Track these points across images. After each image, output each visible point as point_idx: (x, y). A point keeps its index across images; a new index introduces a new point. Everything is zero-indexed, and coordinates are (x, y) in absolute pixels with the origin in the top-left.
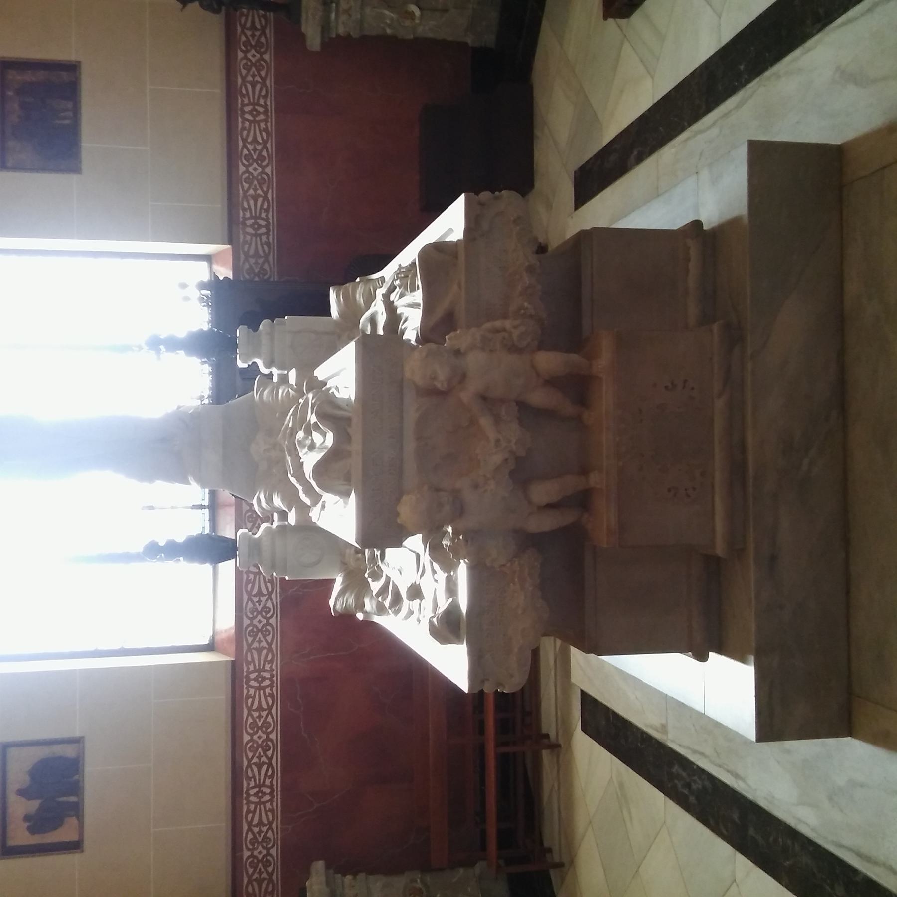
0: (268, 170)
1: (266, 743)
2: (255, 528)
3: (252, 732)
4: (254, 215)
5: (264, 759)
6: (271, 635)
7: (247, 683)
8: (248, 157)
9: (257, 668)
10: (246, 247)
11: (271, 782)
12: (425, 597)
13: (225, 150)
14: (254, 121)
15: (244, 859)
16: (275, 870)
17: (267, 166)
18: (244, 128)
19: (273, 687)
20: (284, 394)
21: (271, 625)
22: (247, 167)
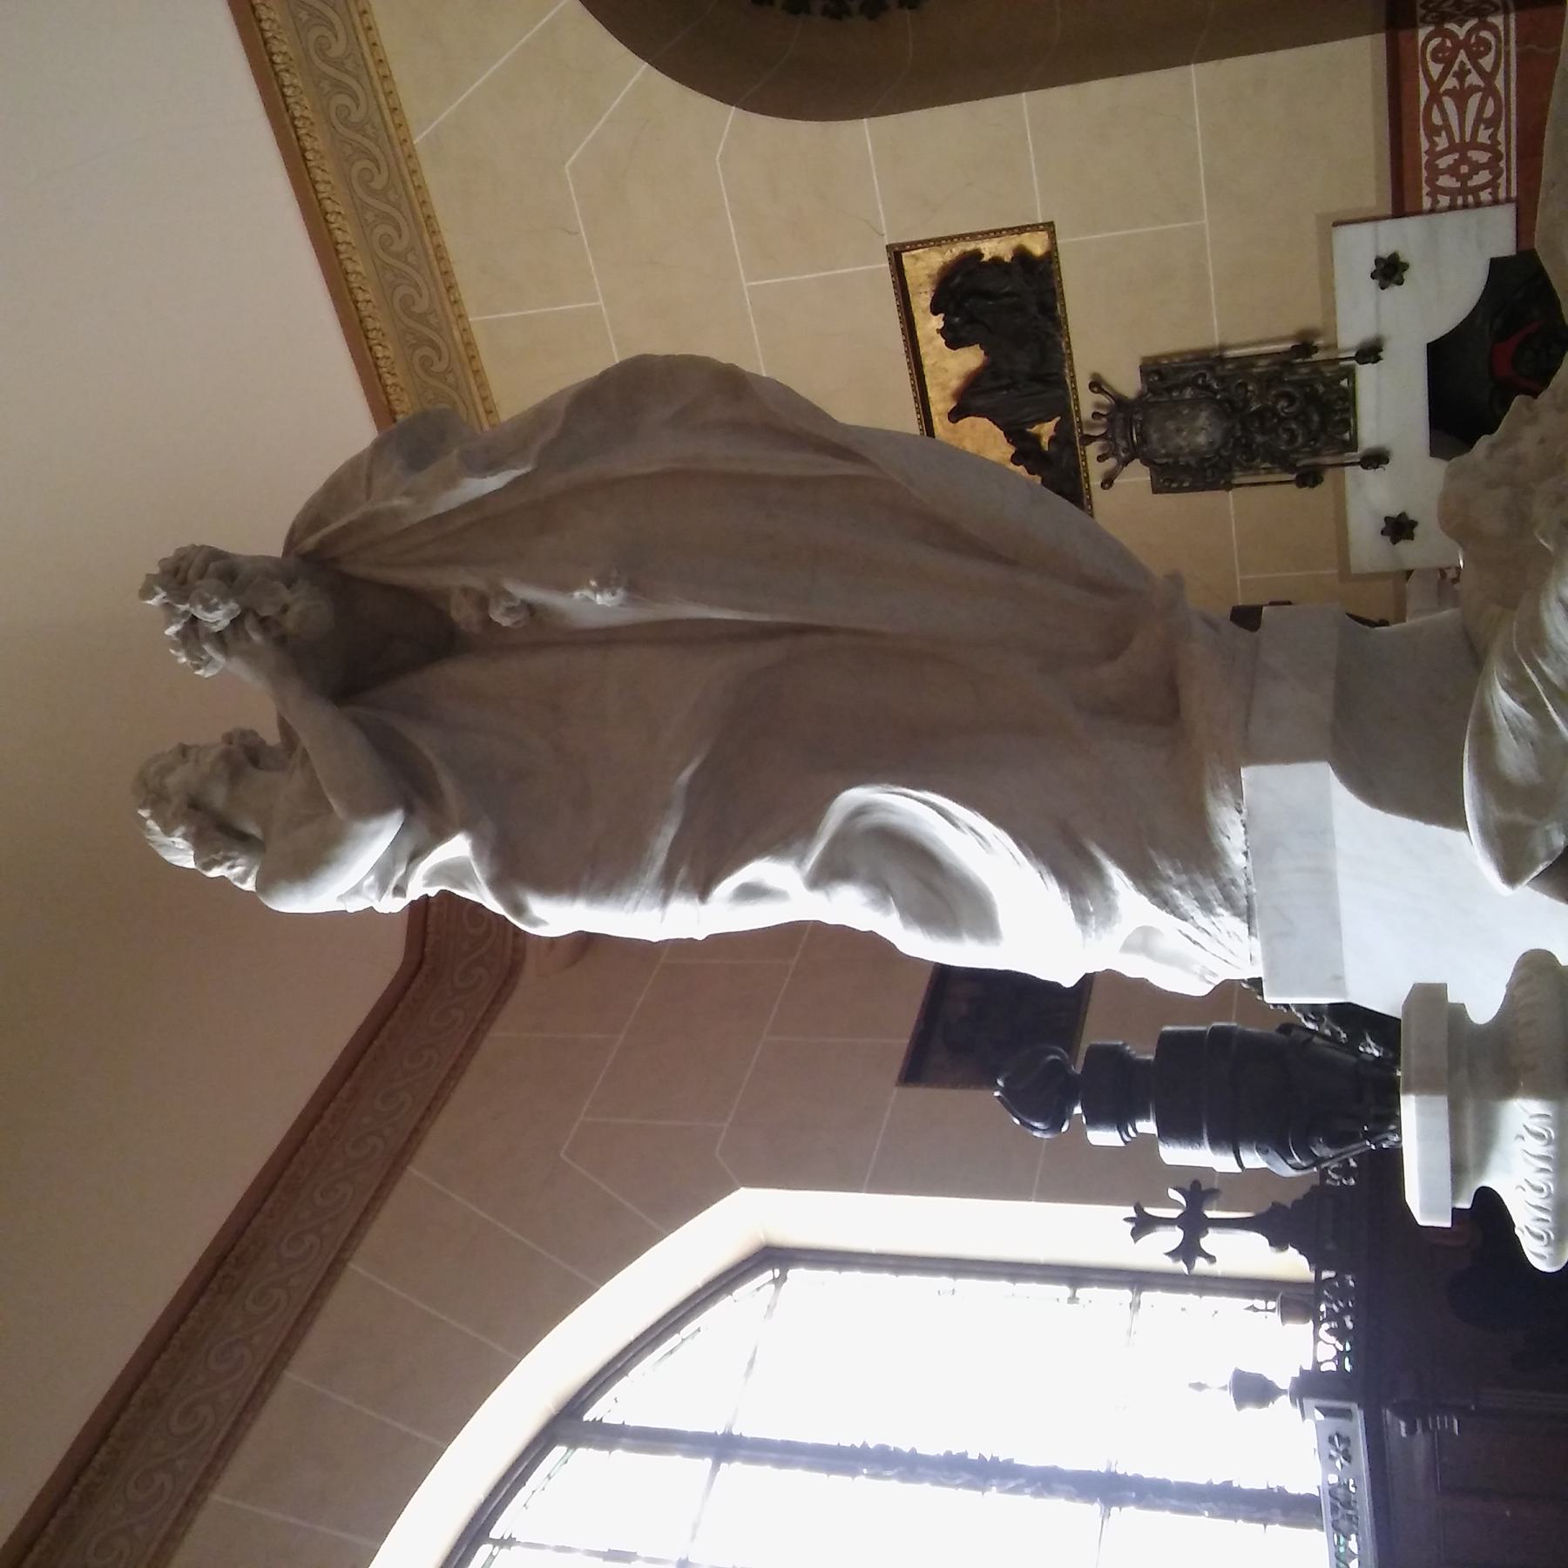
4: (1457, 140)
5: (1473, 79)
6: (1492, 53)
7: (1431, 181)
9: (1457, 140)
11: (1493, 137)
12: (1229, 1479)
15: (1420, 44)
16: (1502, 65)
20: (1439, 1489)
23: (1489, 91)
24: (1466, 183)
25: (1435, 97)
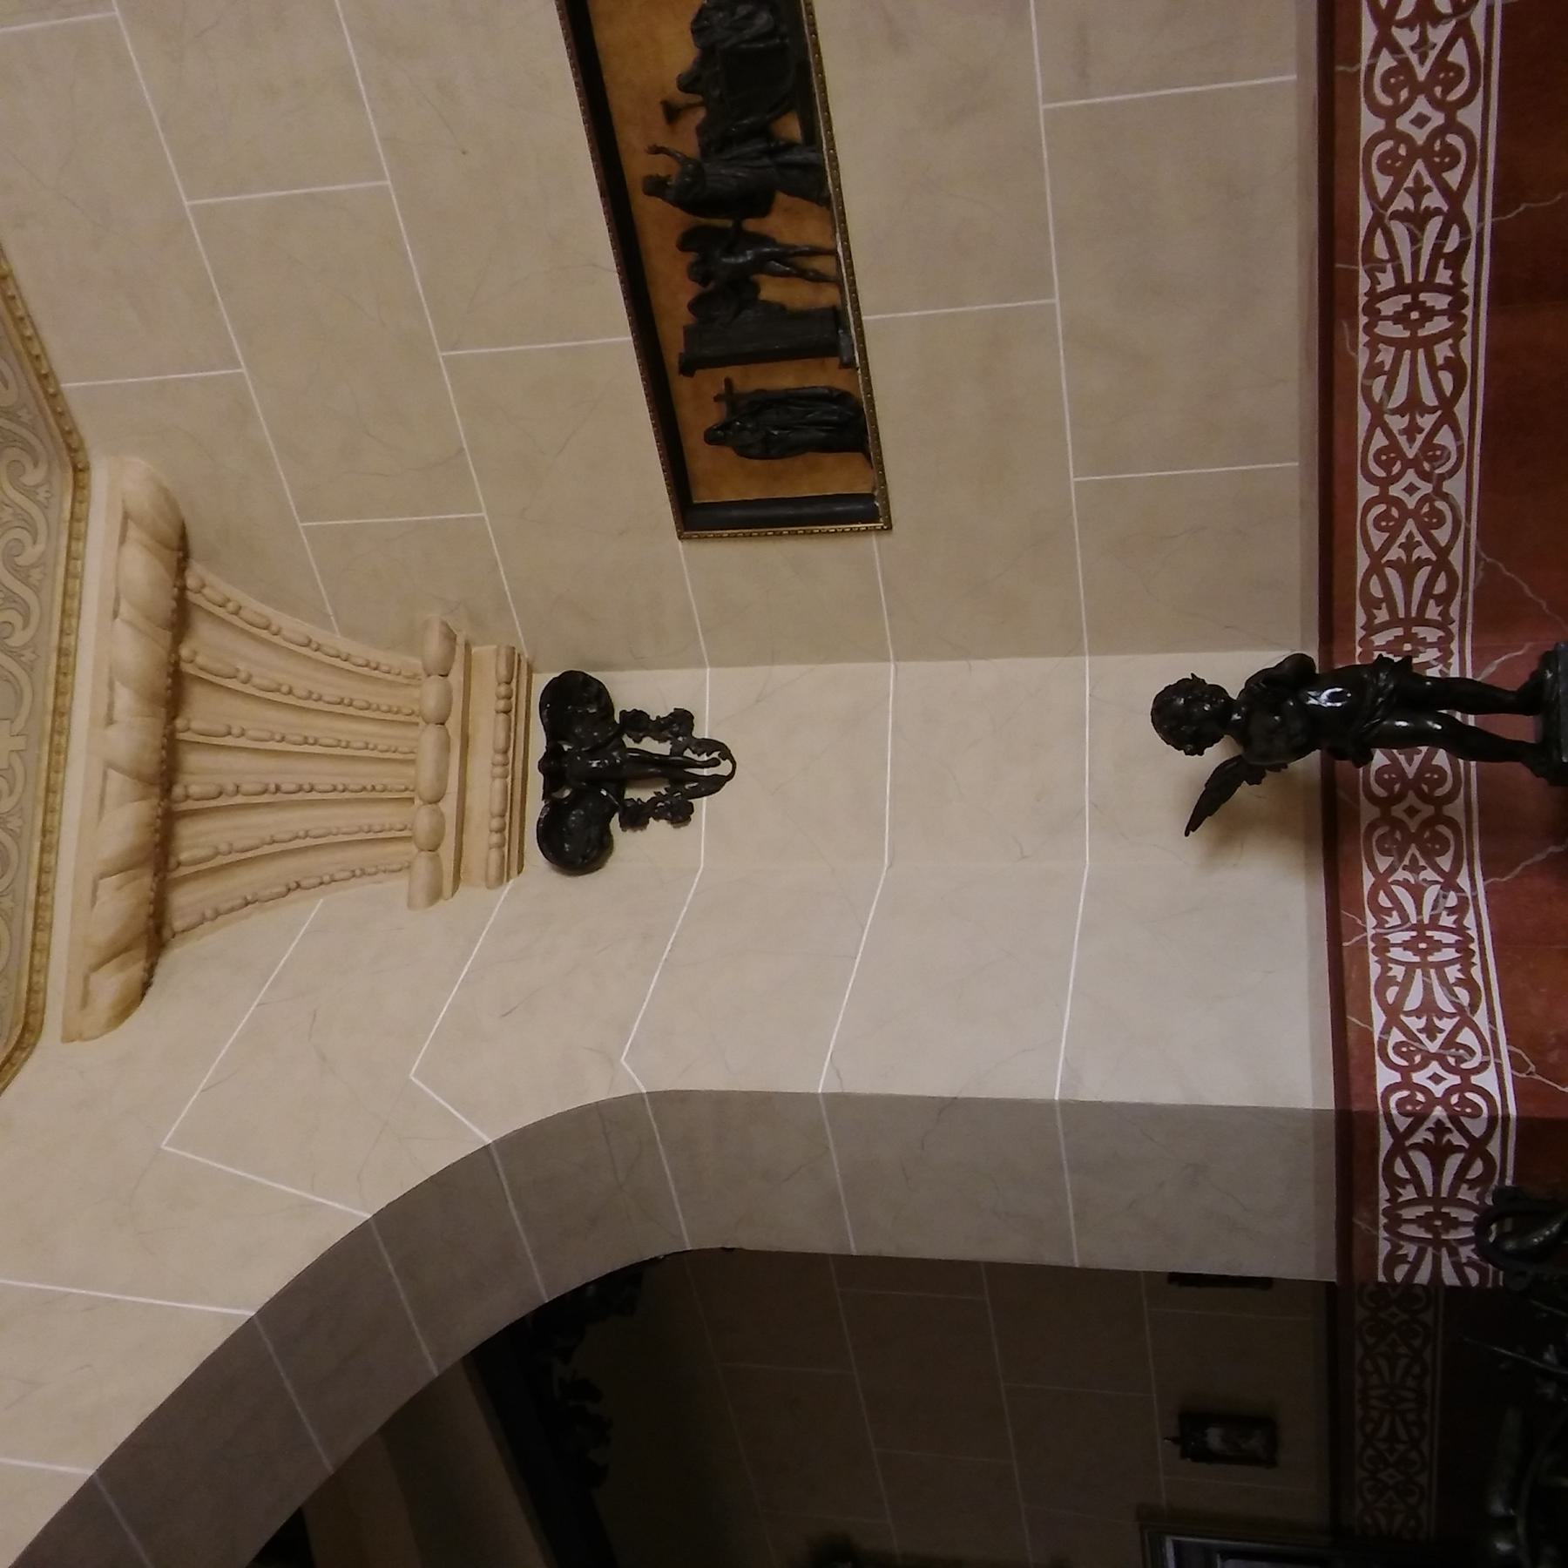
0: (1470, 117)
1: (1443, 143)
2: (1402, 191)
3: (1383, 474)
10: (1379, 384)
14: (1413, 343)
18: (1374, 370)
19: (1464, 334)
23: (1455, 216)
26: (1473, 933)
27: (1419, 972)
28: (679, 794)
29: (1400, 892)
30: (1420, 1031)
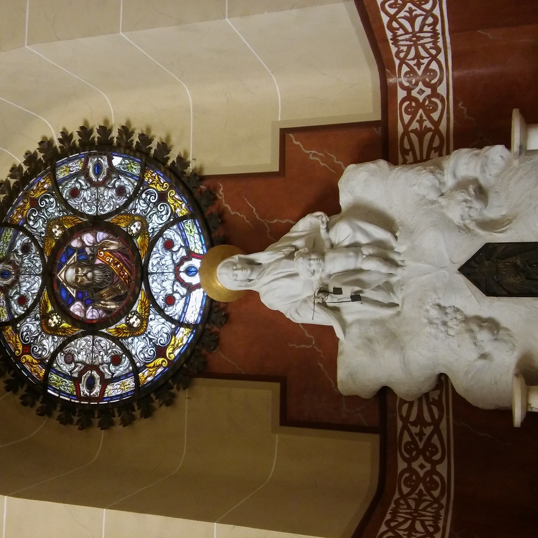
0: (442, 468)
5: (427, 124)
8: (412, 446)
13: (356, 524)
15: (399, 102)
17: (440, 461)
21: (438, 96)
22: (409, 461)
24: (419, 160)
25: (436, 423)
26: (440, 31)
27: (413, 48)
28: (95, 245)
29: (403, 21)
30: (414, 65)
